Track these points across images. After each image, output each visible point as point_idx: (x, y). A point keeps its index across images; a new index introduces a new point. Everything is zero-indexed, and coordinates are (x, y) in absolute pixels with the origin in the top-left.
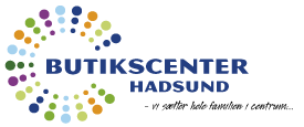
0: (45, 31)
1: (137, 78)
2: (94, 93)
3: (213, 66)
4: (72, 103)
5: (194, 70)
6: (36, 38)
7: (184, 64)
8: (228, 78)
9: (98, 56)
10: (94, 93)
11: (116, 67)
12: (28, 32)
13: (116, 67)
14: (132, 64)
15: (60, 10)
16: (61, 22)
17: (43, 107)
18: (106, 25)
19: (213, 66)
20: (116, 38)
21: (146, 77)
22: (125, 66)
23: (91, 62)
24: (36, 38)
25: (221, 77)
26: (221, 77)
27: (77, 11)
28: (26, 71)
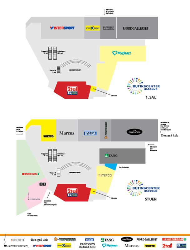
0: (133, 81)
1: (145, 88)
2: (139, 90)
3: (155, 188)
4: (136, 193)
5: (153, 87)
6: (131, 82)
7: (151, 188)
8: (157, 190)
9: (140, 85)
10: (139, 192)
11: (142, 86)
12: (130, 183)
13: (142, 86)
14: (144, 86)
15: (135, 180)
16: (135, 80)
17: (132, 92)
18: (141, 81)
19: (155, 188)
20: (142, 184)
21: (146, 88)
22: (143, 86)
23: (139, 188)
24: (131, 82)
25: (156, 88)
26: (156, 88)
27: (137, 180)
28: (130, 189)
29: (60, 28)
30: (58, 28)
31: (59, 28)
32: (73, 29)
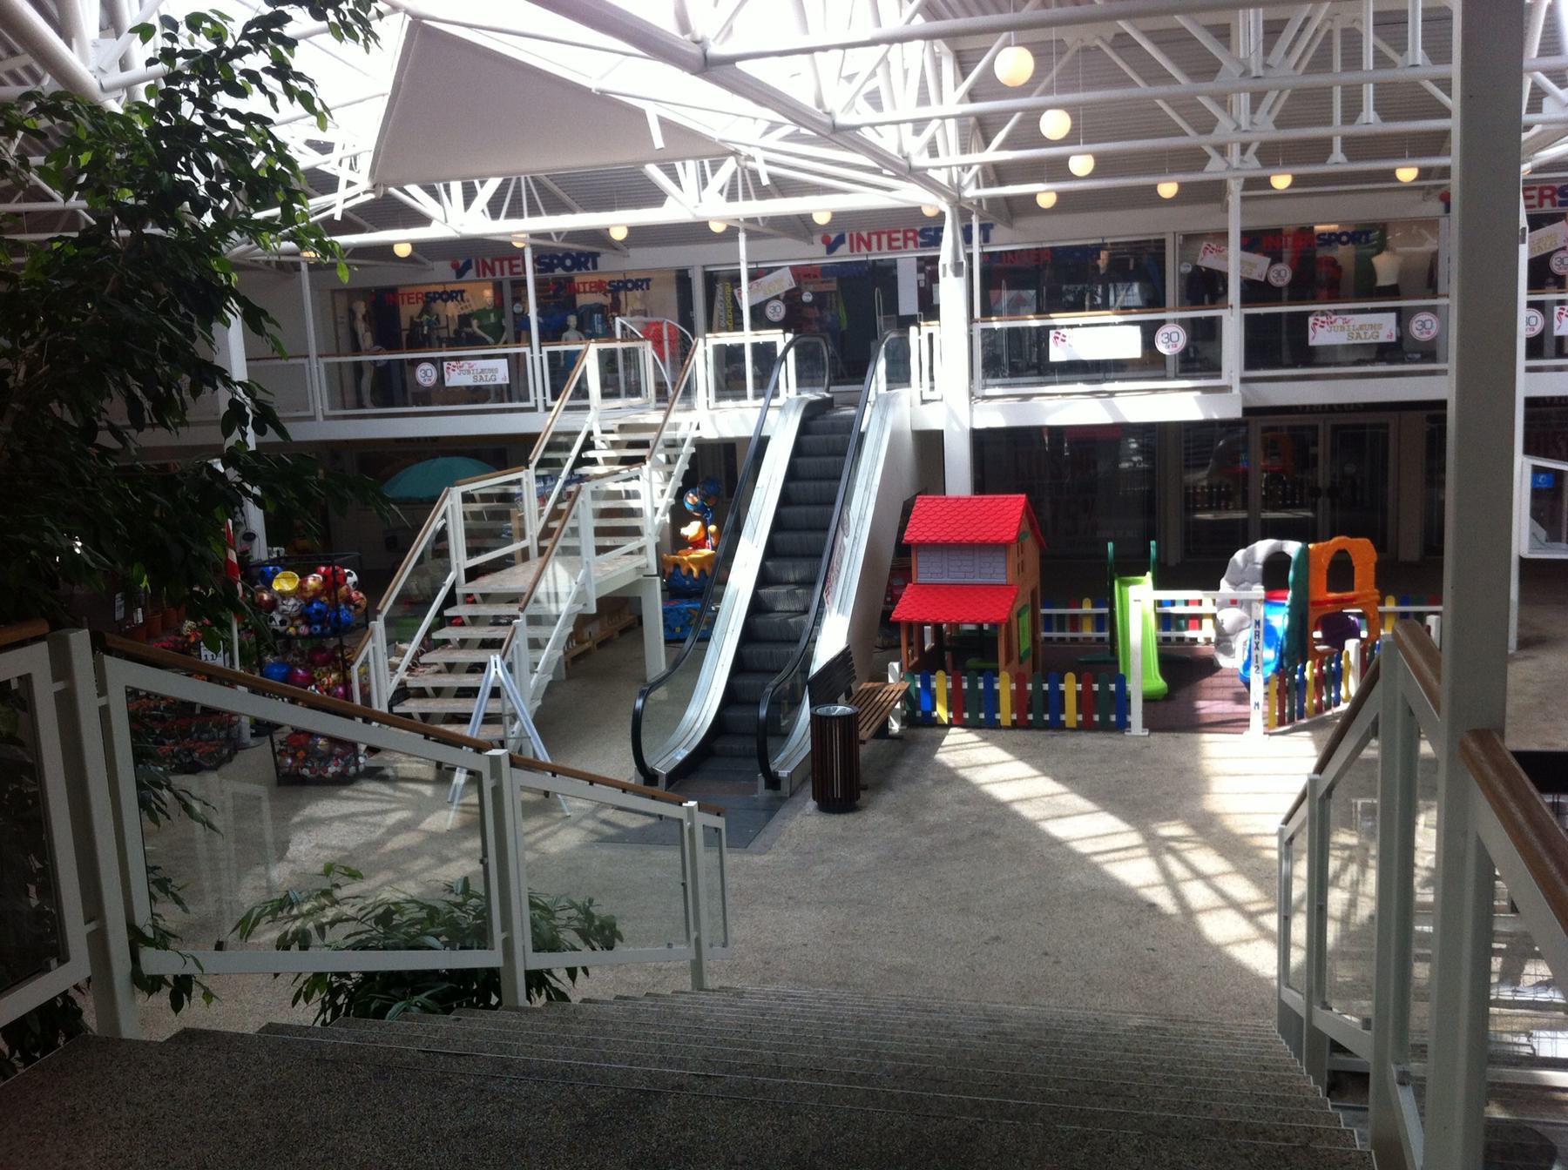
29: (409, 299)
30: (874, 239)
31: (884, 238)
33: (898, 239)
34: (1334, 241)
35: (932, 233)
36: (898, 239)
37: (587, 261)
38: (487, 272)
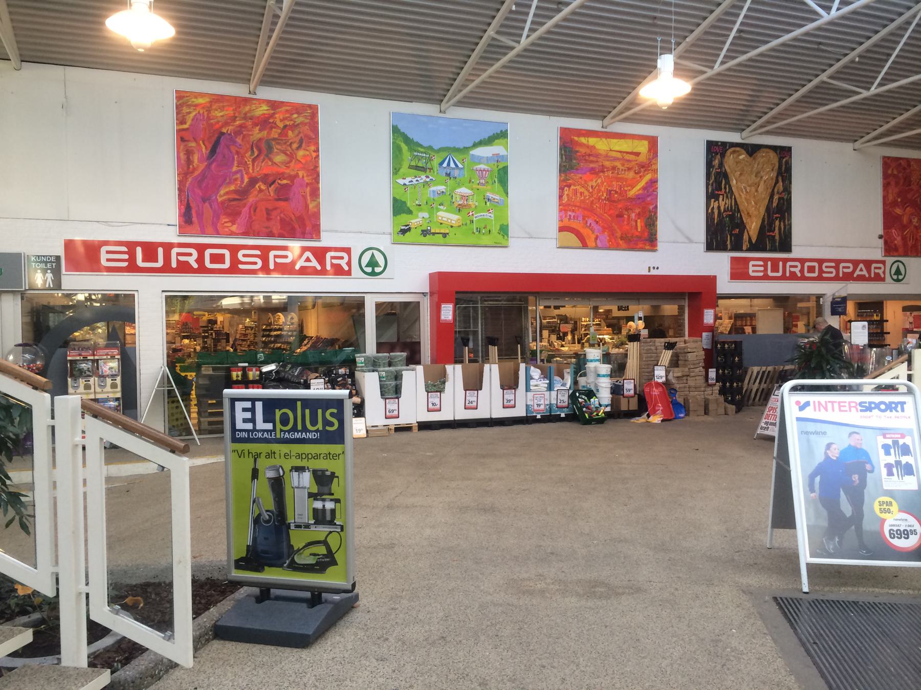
29: (840, 406)
30: (829, 405)
32: (903, 410)
33: (845, 406)
34: (874, 408)
35: (867, 405)
36: (845, 406)
37: (896, 407)
38: (821, 408)
